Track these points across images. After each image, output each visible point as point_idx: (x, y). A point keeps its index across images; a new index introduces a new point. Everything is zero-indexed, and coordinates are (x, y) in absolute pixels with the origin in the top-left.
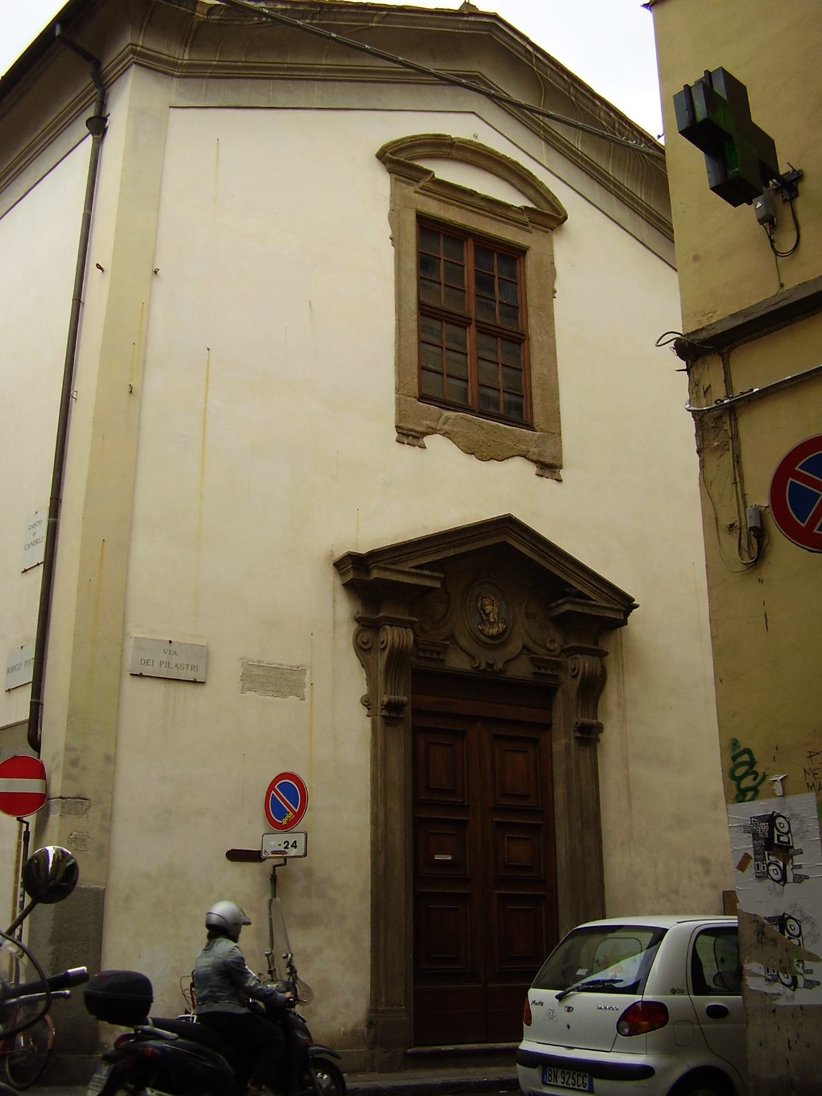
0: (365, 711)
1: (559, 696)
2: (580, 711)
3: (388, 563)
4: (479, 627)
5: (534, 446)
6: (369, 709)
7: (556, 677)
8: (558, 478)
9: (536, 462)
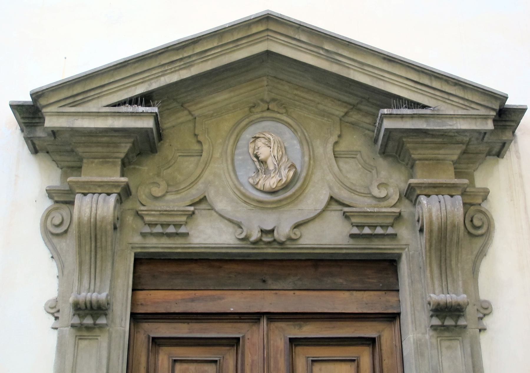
1: (404, 268)
2: (437, 283)
6: (57, 318)
7: (394, 236)
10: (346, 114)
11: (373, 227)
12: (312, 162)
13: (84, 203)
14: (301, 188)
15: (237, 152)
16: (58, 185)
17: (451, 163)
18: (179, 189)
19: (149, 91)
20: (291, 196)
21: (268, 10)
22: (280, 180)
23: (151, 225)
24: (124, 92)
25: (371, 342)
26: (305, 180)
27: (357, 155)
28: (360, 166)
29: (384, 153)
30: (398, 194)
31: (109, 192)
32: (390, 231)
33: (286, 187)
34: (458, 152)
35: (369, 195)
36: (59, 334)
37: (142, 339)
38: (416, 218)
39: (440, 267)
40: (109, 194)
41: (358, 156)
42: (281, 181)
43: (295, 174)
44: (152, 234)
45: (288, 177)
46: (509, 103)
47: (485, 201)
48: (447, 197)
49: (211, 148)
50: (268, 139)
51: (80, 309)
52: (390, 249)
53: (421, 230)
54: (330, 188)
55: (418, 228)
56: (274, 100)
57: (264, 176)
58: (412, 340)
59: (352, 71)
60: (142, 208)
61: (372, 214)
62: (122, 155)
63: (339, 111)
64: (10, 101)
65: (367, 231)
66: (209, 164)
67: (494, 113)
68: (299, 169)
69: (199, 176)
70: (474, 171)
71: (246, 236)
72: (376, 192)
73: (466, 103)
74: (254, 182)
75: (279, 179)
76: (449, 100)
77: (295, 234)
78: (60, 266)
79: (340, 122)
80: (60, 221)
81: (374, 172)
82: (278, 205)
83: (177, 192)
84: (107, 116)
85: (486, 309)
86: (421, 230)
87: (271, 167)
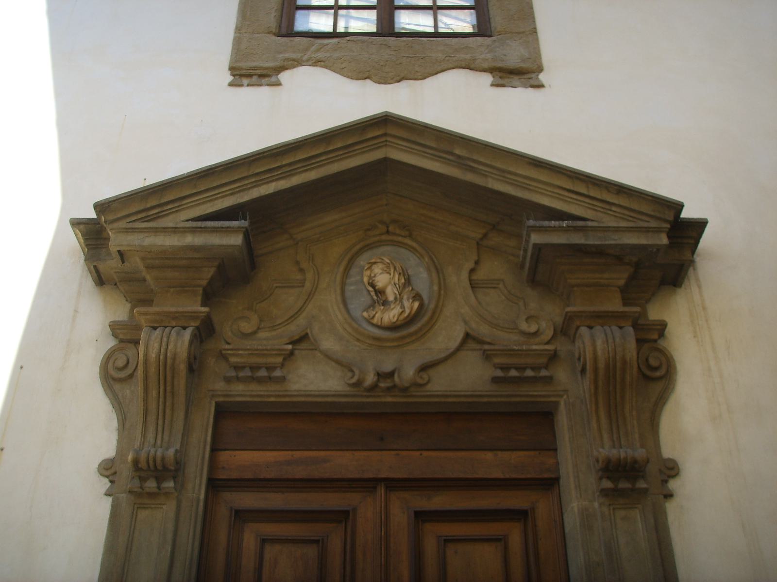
0: (105, 484)
1: (562, 420)
2: (606, 436)
3: (134, 221)
4: (365, 314)
5: (487, 51)
6: (111, 481)
7: (549, 380)
8: (536, 84)
9: (491, 70)
10: (485, 236)
11: (521, 368)
12: (442, 292)
13: (153, 338)
14: (428, 322)
15: (348, 281)
16: (121, 319)
17: (618, 290)
18: (275, 324)
19: (239, 204)
20: (416, 332)
21: (386, 112)
22: (402, 312)
23: (237, 368)
24: (209, 205)
25: (521, 515)
26: (434, 313)
27: (498, 284)
28: (503, 297)
29: (533, 281)
30: (552, 329)
31: (186, 325)
32: (544, 373)
33: (411, 320)
34: (626, 275)
35: (515, 331)
36: (113, 501)
37: (223, 514)
38: (577, 355)
39: (609, 416)
40: (184, 328)
41: (501, 286)
42: (403, 314)
43: (421, 306)
44: (238, 379)
45: (412, 308)
46: (684, 214)
47: (662, 338)
48: (615, 328)
49: (317, 276)
50: (386, 263)
51: (141, 469)
52: (544, 396)
53: (583, 371)
54: (466, 322)
55: (579, 369)
56: (395, 221)
57: (382, 307)
58: (576, 510)
59: (490, 180)
60: (227, 347)
61: (520, 353)
62: (204, 283)
63: (476, 233)
64: (71, 219)
65: (513, 373)
66: (313, 296)
67: (668, 226)
68: (426, 301)
69: (299, 311)
70: (647, 302)
71: (358, 380)
72: (524, 326)
73: (632, 214)
74: (369, 316)
75: (401, 310)
76: (611, 210)
77: (421, 378)
78: (121, 417)
79: (478, 249)
80: (125, 362)
81: (521, 303)
82: (401, 343)
83: (273, 328)
84: (185, 232)
85: (672, 469)
86: (583, 371)
87: (391, 298)
